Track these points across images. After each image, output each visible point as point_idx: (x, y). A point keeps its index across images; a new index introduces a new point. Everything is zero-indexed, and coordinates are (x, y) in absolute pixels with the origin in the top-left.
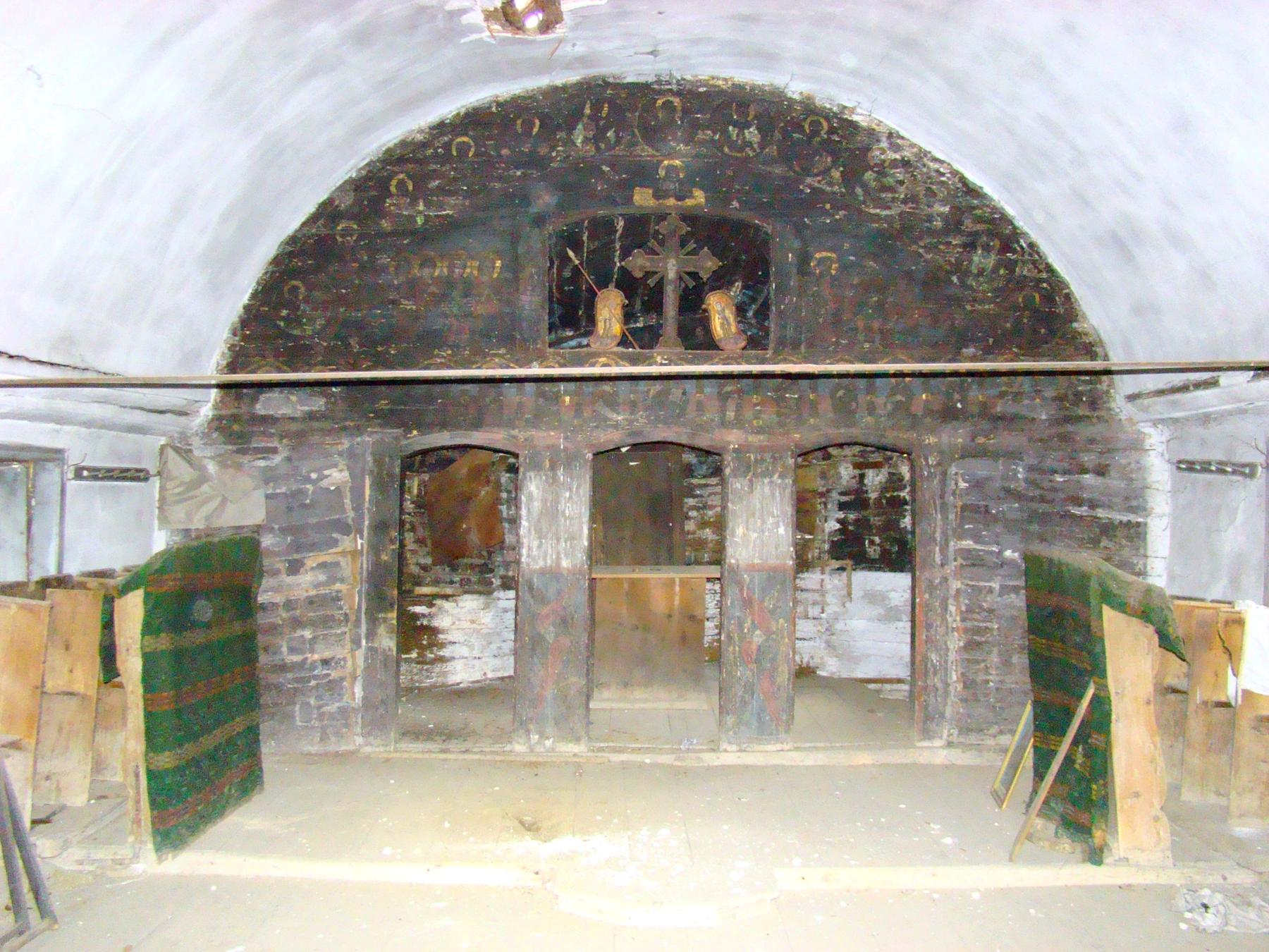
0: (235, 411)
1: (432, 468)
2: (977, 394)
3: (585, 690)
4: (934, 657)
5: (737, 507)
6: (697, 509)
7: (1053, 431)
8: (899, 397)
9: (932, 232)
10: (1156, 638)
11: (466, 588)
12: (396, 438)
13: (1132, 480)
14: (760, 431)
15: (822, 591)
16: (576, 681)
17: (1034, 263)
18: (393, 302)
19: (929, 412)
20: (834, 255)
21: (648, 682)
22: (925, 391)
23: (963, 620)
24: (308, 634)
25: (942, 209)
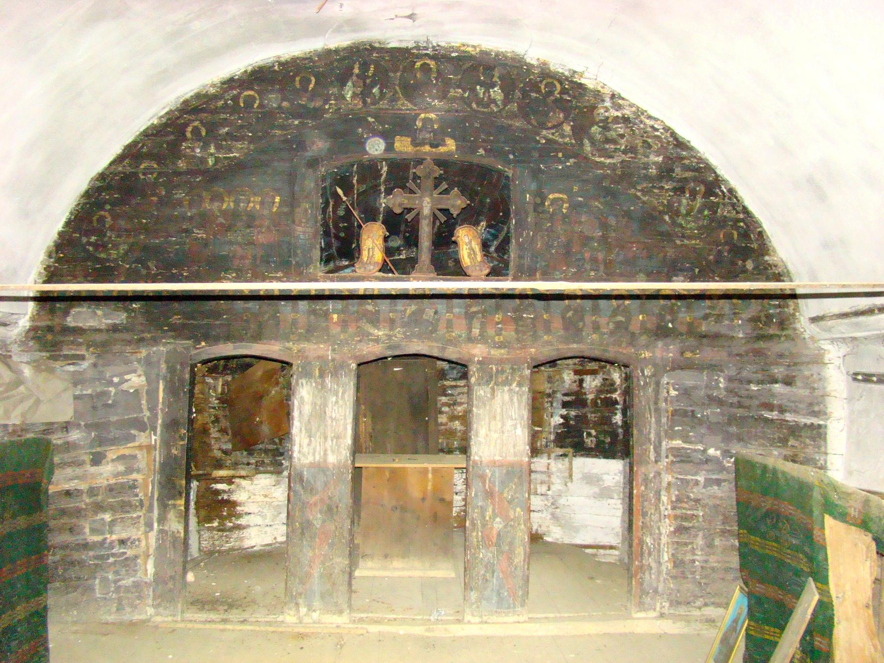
0: (49, 323)
1: (233, 372)
2: (685, 315)
3: (348, 569)
4: (648, 540)
5: (481, 412)
6: (449, 405)
8: (620, 318)
9: (647, 178)
10: (873, 546)
12: (187, 349)
13: (814, 389)
14: (501, 345)
15: (548, 472)
16: (341, 562)
17: (733, 206)
18: (186, 231)
19: (645, 330)
20: (565, 197)
21: (405, 555)
22: (641, 313)
23: (673, 508)
24: (107, 517)
25: (656, 159)
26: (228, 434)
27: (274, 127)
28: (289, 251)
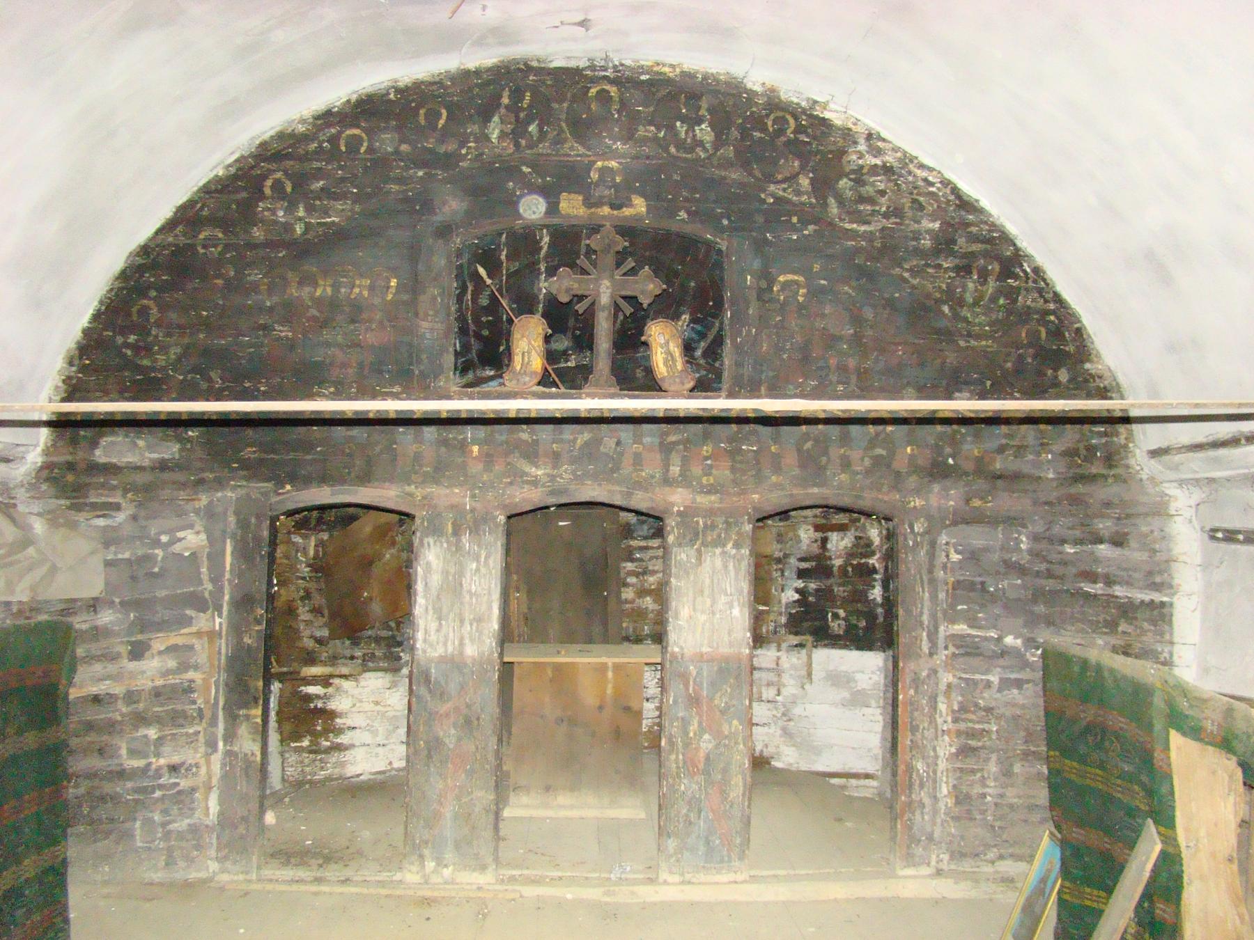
0: (70, 458)
1: (331, 527)
2: (972, 446)
3: (493, 807)
4: (920, 765)
6: (637, 575)
7: (1063, 491)
8: (880, 451)
9: (918, 252)
10: (1239, 774)
11: (368, 664)
12: (265, 494)
13: (1155, 551)
14: (711, 490)
15: (777, 670)
16: (483, 796)
17: (1040, 291)
18: (265, 327)
19: (915, 468)
20: (801, 279)
21: (574, 787)
22: (909, 443)
23: (955, 721)
24: (152, 733)
25: (931, 225)
26: (323, 616)
27: (388, 180)
28: (410, 356)
